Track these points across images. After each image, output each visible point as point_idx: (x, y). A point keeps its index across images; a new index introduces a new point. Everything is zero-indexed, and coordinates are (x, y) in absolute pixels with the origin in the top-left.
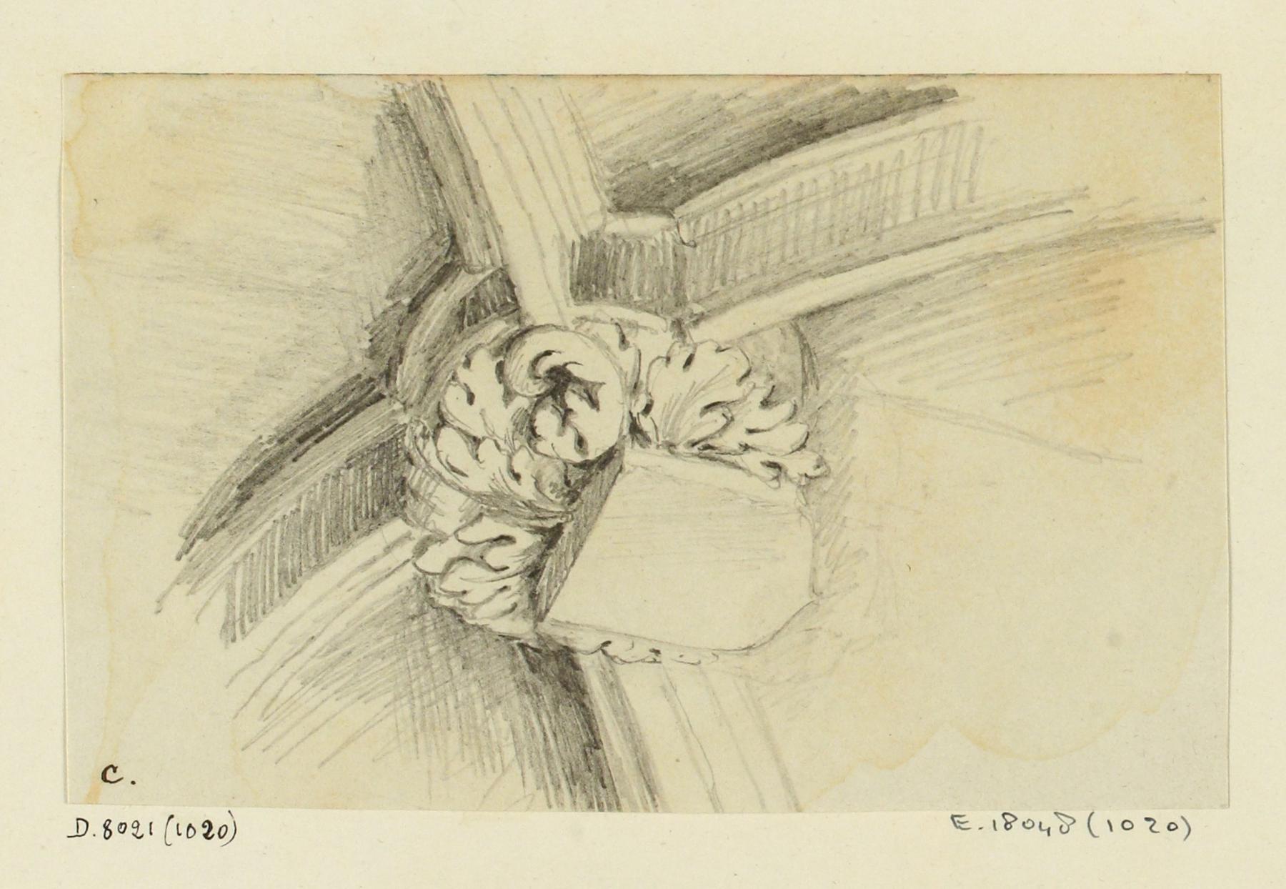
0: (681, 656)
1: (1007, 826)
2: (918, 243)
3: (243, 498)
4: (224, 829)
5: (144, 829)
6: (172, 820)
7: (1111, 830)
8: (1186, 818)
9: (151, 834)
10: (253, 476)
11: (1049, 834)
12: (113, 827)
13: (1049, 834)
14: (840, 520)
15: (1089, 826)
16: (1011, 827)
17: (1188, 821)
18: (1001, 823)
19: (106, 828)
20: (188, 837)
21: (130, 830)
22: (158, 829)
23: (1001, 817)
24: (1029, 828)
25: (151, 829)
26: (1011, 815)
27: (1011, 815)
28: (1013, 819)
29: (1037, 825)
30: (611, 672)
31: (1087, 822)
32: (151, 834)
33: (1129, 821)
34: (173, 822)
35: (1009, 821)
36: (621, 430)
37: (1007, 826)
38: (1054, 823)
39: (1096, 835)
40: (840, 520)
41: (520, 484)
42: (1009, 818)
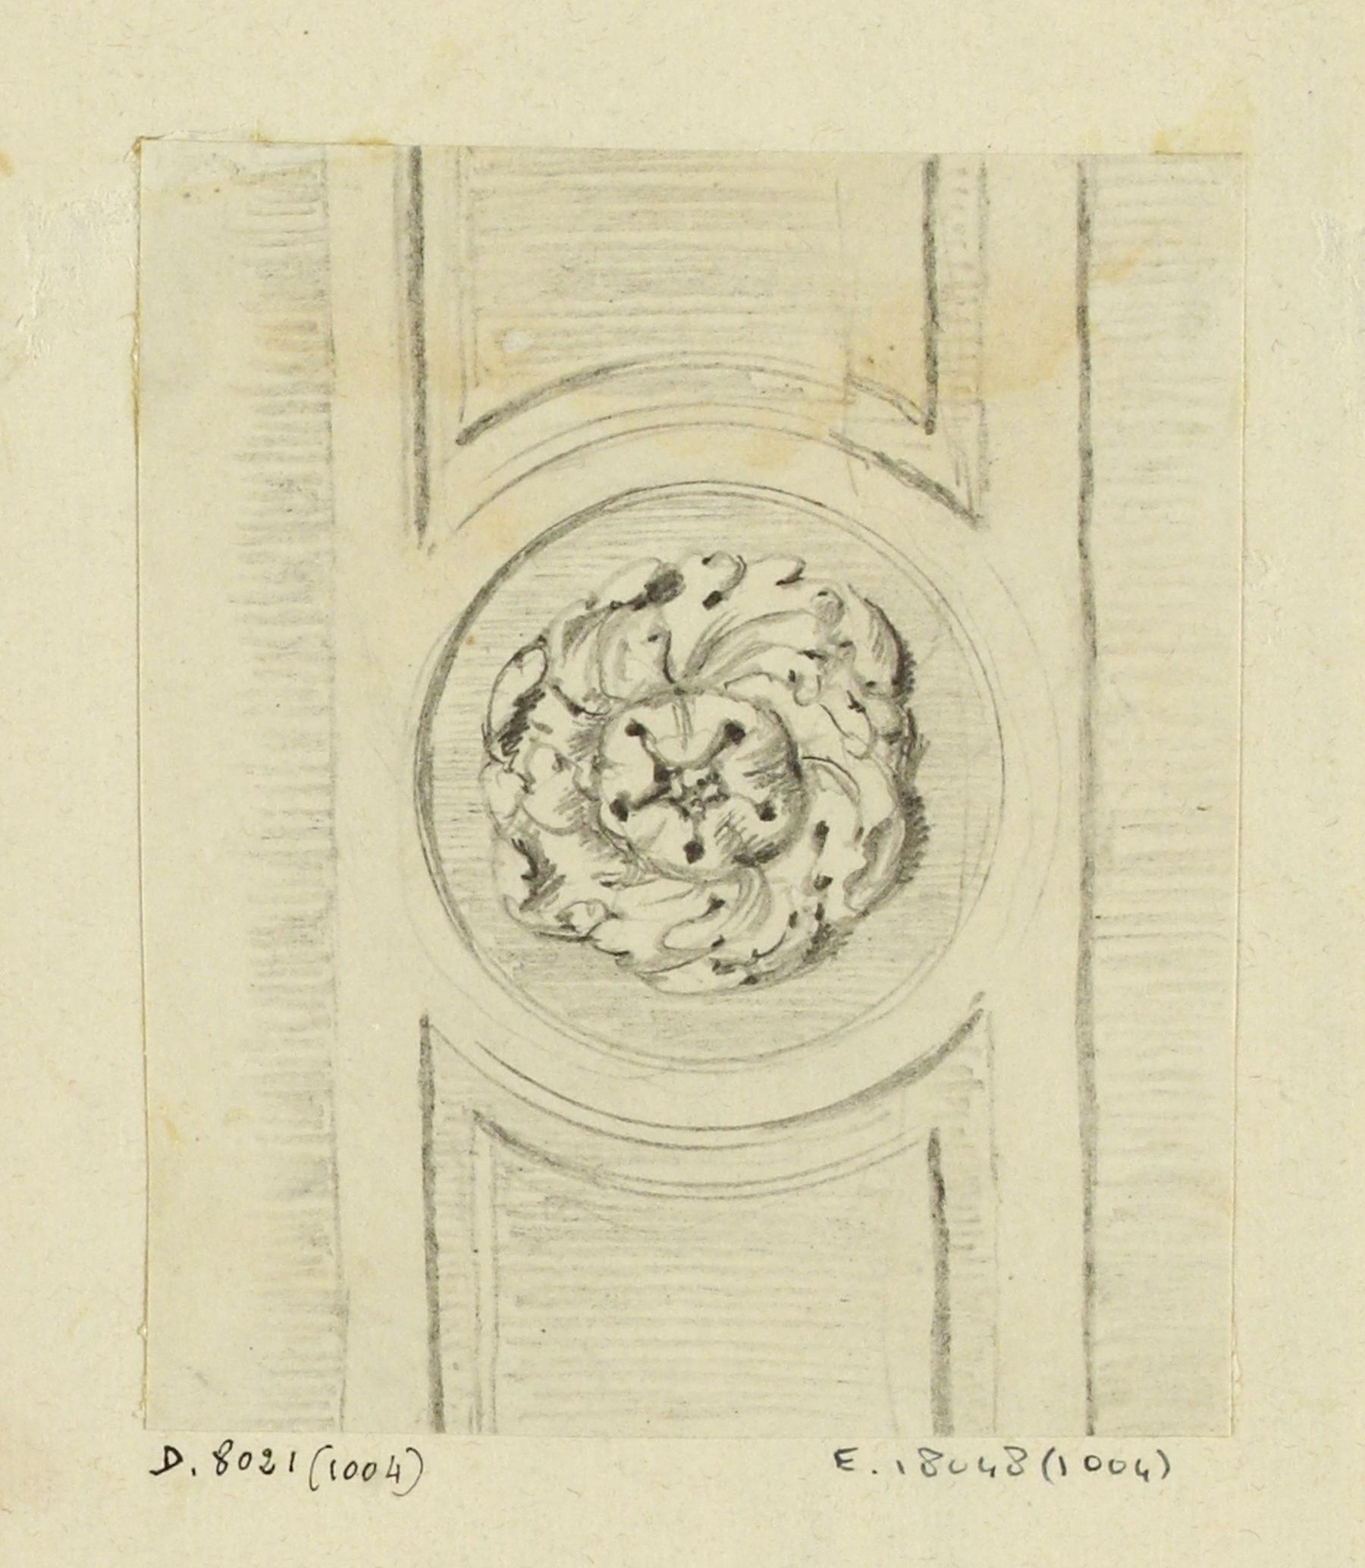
2: (572, 456)
3: (514, 1142)
4: (244, 1464)
7: (1064, 1473)
8: (1166, 1453)
9: (291, 1469)
11: (992, 1475)
12: (232, 1458)
13: (992, 1475)
14: (940, 1428)
17: (310, 1466)
18: (913, 1463)
22: (302, 1464)
24: (1119, 1472)
25: (292, 1461)
29: (1131, 1468)
31: (422, 1456)
32: (291, 1469)
33: (1094, 1457)
34: (326, 1456)
38: (1001, 1461)
40: (940, 1428)
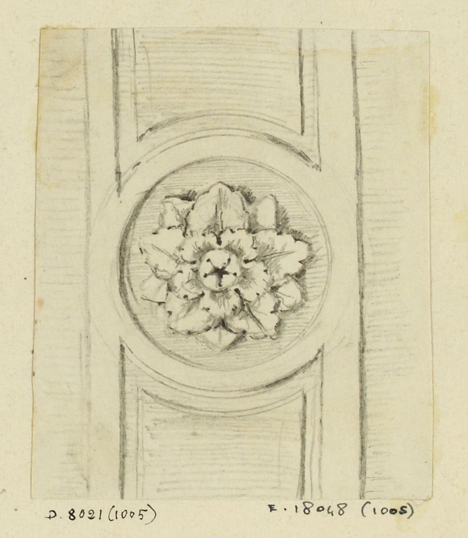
0: (323, 31)
1: (307, 511)
5: (97, 515)
6: (114, 508)
10: (186, 200)
15: (363, 507)
16: (344, 512)
18: (301, 508)
19: (71, 514)
20: (123, 518)
21: (87, 515)
23: (124, 519)
26: (309, 502)
27: (309, 502)
28: (311, 505)
30: (227, 46)
31: (363, 505)
33: (54, 517)
35: (308, 507)
36: (297, 287)
37: (307, 511)
39: (365, 515)
41: (266, 298)
42: (308, 505)
